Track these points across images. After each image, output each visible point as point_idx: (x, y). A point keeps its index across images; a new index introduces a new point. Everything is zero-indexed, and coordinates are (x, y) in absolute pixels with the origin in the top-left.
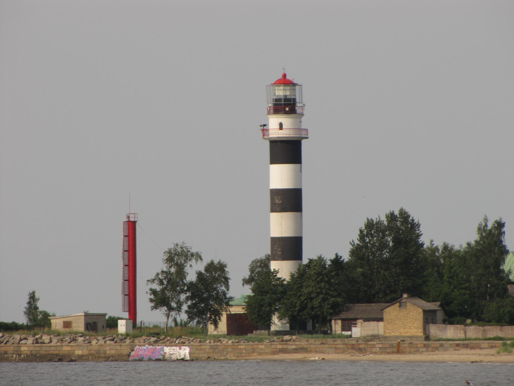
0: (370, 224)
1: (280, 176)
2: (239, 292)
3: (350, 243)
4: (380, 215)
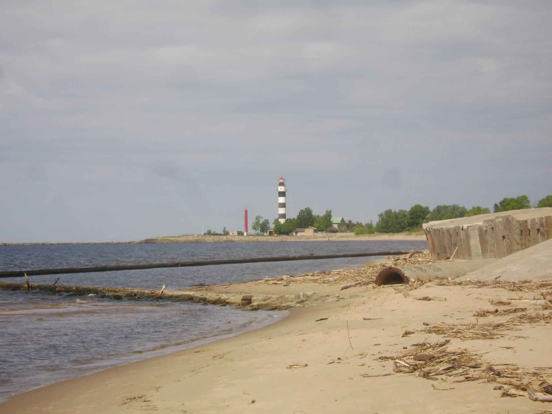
0: (301, 211)
1: (281, 200)
2: (272, 226)
3: (145, 396)
4: (303, 209)
